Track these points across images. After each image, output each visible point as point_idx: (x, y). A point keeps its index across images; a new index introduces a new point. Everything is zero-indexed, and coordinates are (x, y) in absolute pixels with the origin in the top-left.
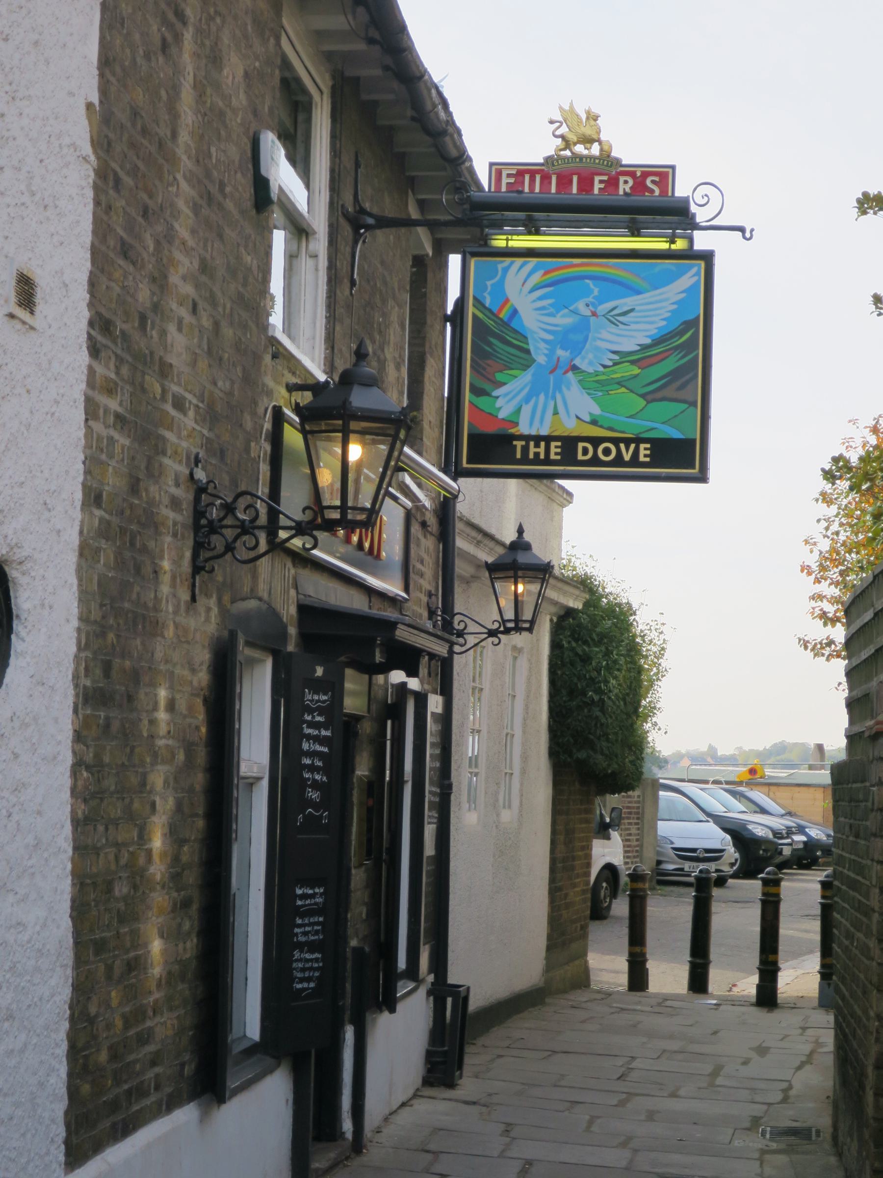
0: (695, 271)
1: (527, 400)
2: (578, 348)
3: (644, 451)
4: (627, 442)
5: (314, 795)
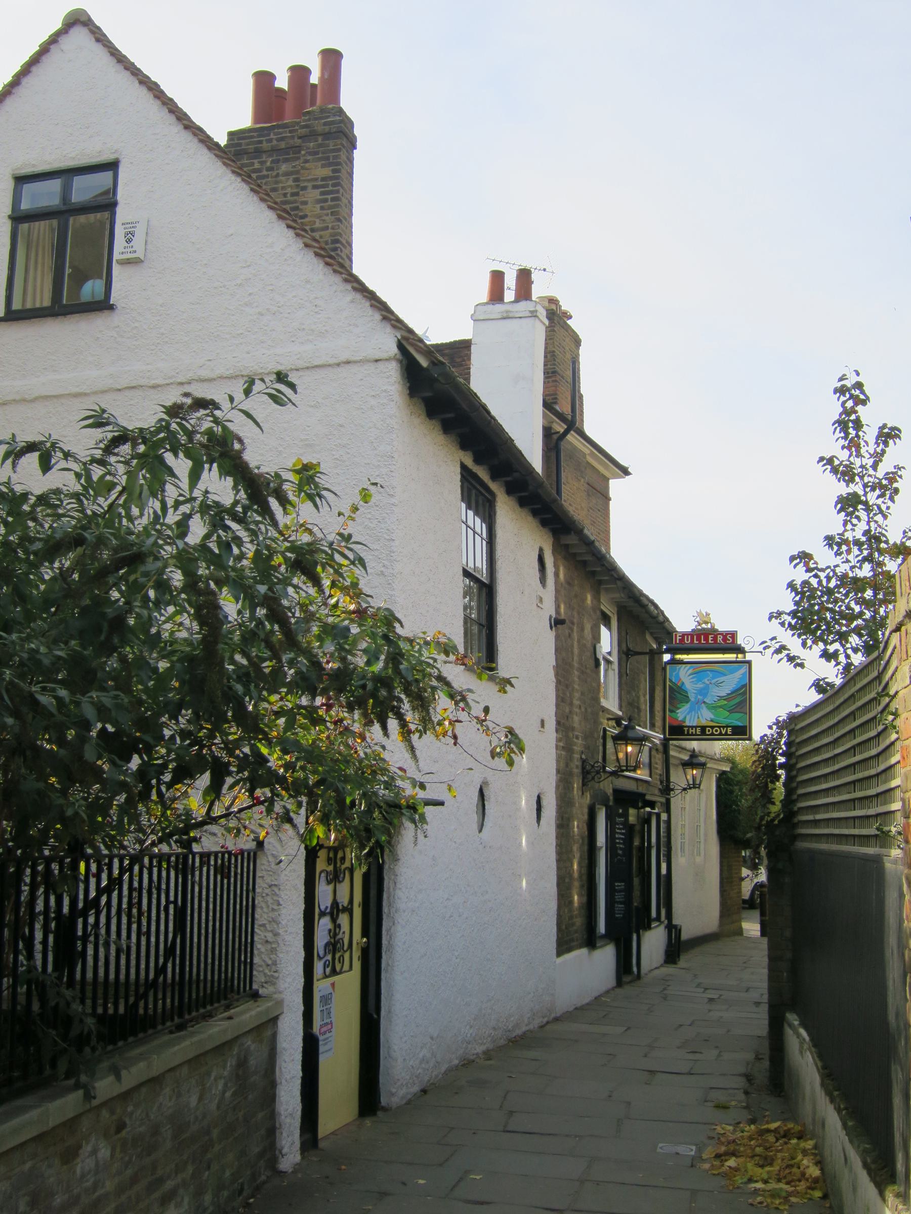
0: (745, 668)
1: (688, 714)
2: (705, 695)
3: (729, 730)
4: (723, 727)
5: (620, 852)
